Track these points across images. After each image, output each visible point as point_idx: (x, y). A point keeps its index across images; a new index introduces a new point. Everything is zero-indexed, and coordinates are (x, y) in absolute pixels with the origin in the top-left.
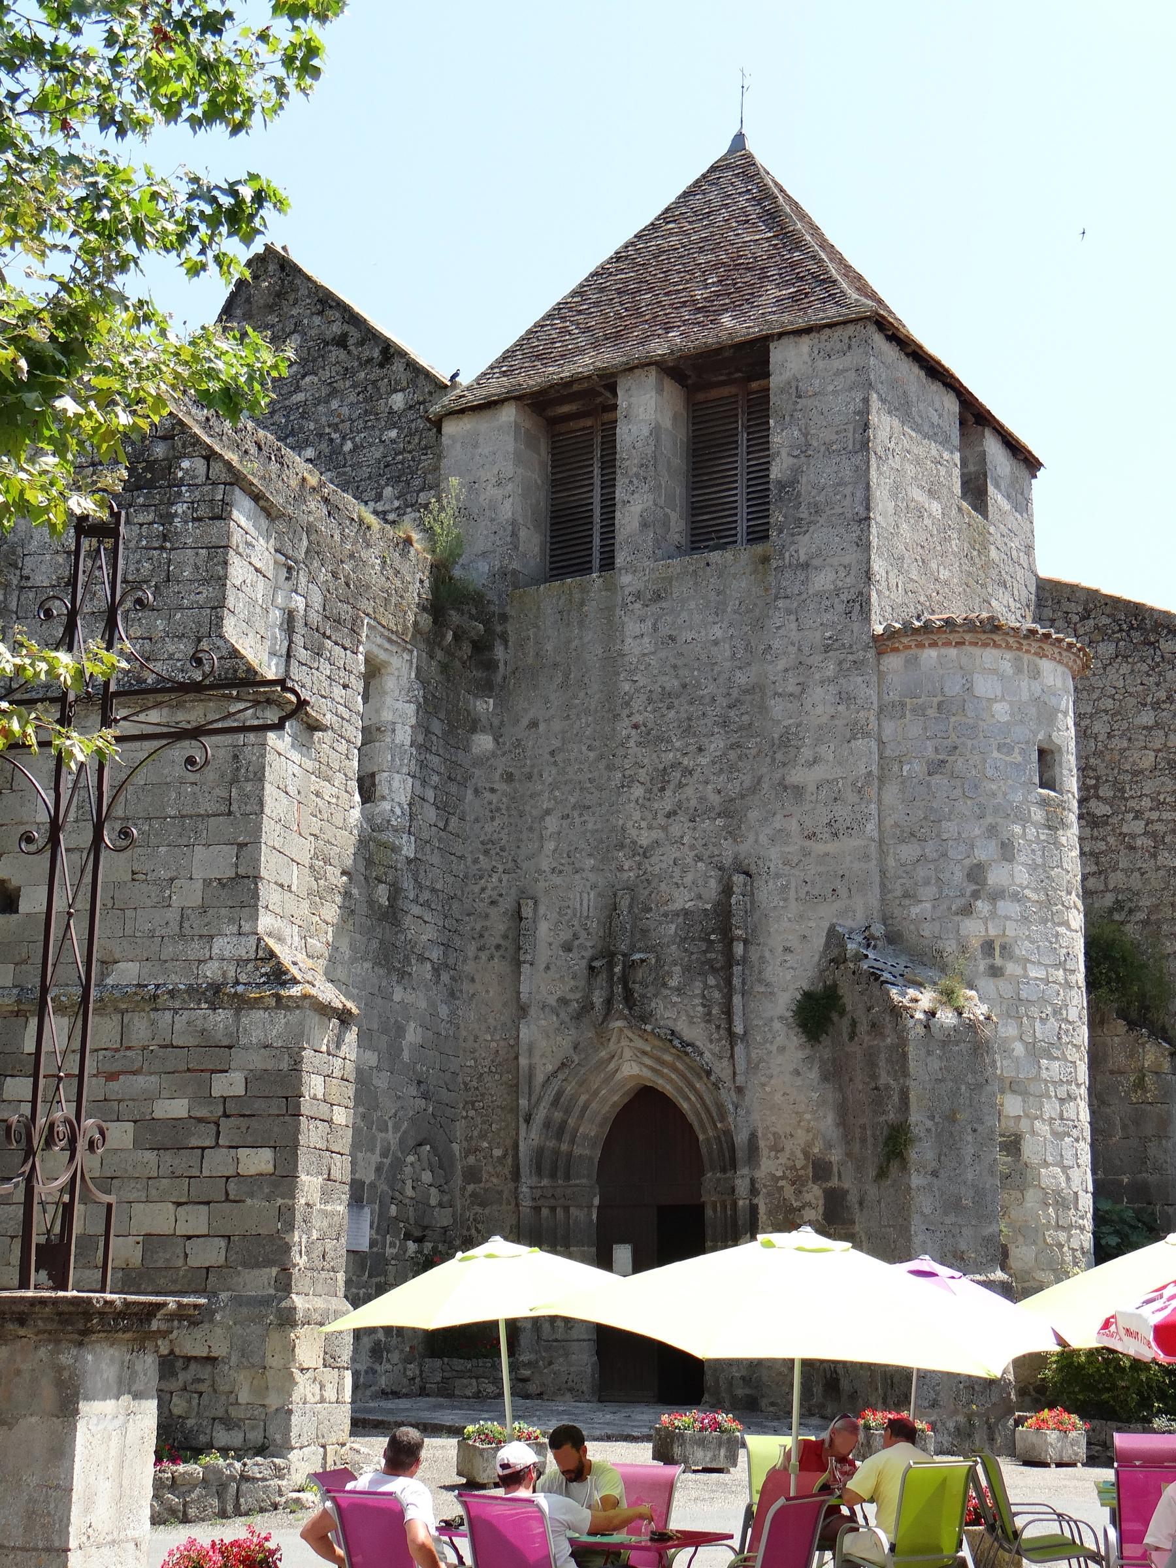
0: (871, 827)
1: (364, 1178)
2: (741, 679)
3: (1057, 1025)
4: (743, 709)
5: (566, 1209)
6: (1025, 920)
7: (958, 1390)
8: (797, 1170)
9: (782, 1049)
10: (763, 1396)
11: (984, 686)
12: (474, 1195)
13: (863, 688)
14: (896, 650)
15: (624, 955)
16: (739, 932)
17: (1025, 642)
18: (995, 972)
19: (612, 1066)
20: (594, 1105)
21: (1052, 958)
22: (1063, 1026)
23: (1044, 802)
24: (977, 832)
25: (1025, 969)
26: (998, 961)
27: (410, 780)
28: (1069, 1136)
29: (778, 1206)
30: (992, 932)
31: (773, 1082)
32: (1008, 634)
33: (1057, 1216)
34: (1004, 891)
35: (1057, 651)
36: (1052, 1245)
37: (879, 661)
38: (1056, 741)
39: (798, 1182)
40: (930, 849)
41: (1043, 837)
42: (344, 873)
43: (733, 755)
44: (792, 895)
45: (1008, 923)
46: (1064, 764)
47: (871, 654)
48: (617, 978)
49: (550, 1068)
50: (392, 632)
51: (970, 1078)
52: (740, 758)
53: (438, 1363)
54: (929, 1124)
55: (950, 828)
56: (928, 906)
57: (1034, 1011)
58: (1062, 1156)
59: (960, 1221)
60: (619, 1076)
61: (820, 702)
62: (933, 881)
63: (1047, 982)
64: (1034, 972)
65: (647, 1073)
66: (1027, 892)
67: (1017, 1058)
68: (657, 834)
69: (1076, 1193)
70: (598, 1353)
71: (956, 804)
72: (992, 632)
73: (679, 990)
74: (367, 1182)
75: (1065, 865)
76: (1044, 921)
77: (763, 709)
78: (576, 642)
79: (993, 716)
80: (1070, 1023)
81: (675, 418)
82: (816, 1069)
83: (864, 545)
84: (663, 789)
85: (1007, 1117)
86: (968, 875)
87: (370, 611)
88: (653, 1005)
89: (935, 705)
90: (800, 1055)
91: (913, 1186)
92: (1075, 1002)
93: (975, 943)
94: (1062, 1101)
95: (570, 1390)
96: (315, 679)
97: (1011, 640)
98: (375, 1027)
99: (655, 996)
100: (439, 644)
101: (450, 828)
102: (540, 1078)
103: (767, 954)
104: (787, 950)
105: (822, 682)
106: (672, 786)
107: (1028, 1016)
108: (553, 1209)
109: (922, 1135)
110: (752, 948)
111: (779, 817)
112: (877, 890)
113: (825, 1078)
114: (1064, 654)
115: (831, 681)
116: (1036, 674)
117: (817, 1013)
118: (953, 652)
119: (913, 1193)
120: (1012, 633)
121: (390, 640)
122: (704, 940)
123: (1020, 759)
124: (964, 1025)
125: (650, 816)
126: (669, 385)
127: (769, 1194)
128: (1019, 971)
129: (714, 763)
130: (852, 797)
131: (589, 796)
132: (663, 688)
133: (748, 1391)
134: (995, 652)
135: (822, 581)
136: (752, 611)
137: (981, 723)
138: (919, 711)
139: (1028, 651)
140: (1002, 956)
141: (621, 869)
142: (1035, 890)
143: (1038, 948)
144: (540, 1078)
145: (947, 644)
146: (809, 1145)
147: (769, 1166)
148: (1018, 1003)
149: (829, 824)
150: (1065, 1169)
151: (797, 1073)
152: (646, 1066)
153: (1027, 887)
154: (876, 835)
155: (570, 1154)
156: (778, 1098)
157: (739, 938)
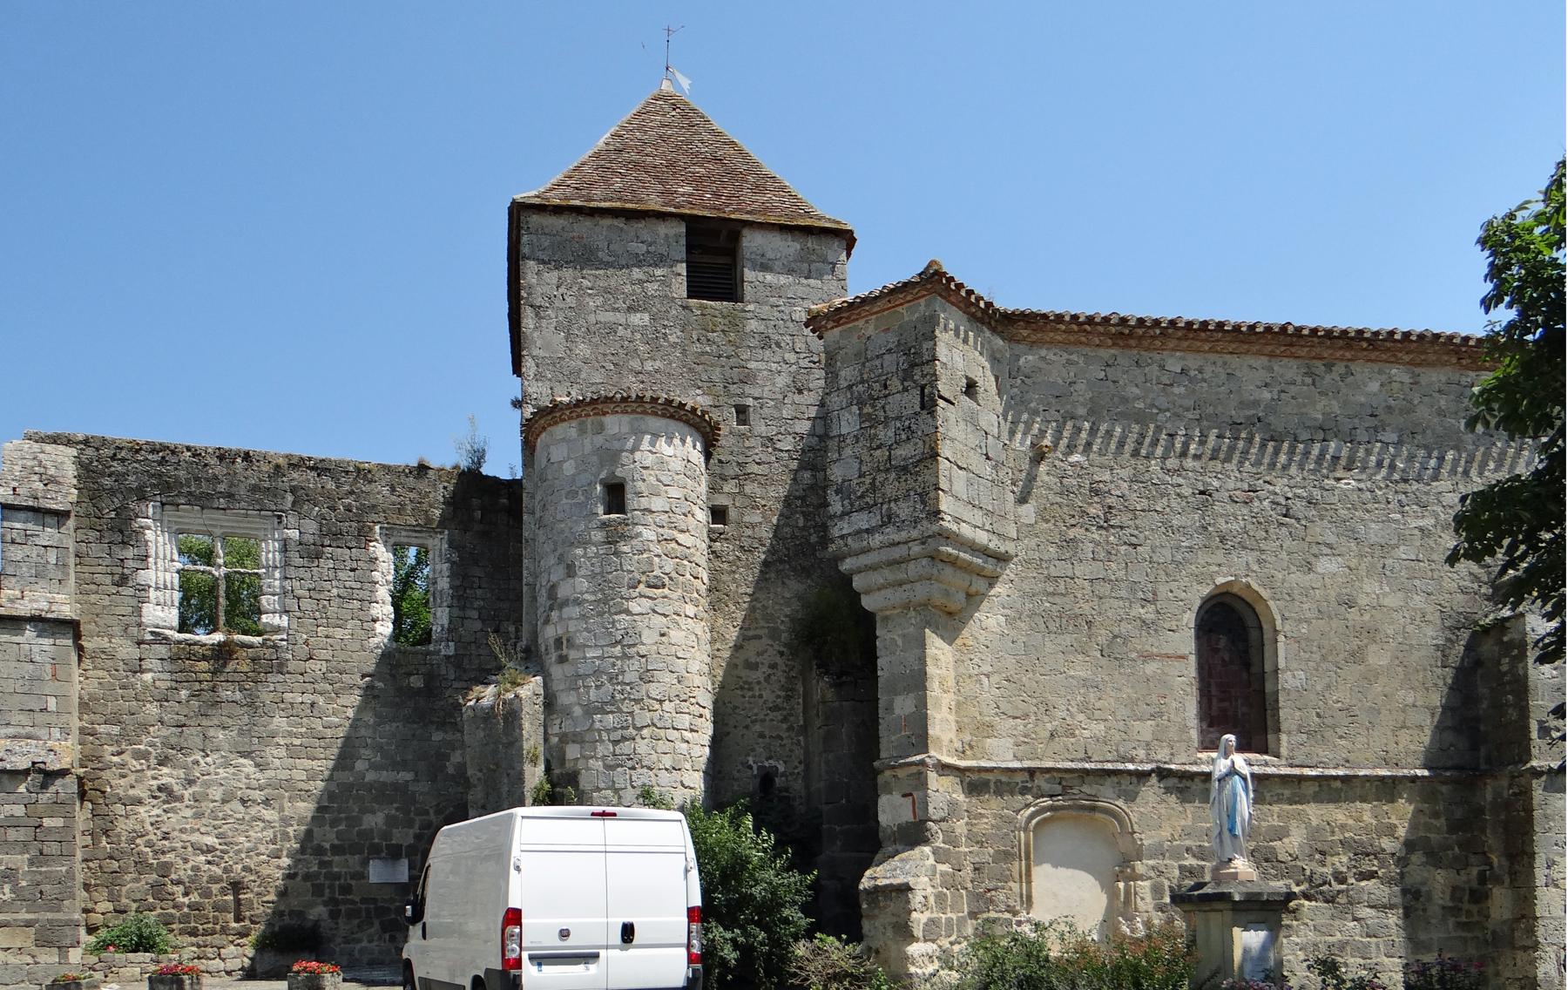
6: (584, 617)
26: (565, 652)
63: (601, 658)
66: (587, 596)
76: (601, 614)
134: (564, 424)
142: (594, 593)
150: (616, 791)
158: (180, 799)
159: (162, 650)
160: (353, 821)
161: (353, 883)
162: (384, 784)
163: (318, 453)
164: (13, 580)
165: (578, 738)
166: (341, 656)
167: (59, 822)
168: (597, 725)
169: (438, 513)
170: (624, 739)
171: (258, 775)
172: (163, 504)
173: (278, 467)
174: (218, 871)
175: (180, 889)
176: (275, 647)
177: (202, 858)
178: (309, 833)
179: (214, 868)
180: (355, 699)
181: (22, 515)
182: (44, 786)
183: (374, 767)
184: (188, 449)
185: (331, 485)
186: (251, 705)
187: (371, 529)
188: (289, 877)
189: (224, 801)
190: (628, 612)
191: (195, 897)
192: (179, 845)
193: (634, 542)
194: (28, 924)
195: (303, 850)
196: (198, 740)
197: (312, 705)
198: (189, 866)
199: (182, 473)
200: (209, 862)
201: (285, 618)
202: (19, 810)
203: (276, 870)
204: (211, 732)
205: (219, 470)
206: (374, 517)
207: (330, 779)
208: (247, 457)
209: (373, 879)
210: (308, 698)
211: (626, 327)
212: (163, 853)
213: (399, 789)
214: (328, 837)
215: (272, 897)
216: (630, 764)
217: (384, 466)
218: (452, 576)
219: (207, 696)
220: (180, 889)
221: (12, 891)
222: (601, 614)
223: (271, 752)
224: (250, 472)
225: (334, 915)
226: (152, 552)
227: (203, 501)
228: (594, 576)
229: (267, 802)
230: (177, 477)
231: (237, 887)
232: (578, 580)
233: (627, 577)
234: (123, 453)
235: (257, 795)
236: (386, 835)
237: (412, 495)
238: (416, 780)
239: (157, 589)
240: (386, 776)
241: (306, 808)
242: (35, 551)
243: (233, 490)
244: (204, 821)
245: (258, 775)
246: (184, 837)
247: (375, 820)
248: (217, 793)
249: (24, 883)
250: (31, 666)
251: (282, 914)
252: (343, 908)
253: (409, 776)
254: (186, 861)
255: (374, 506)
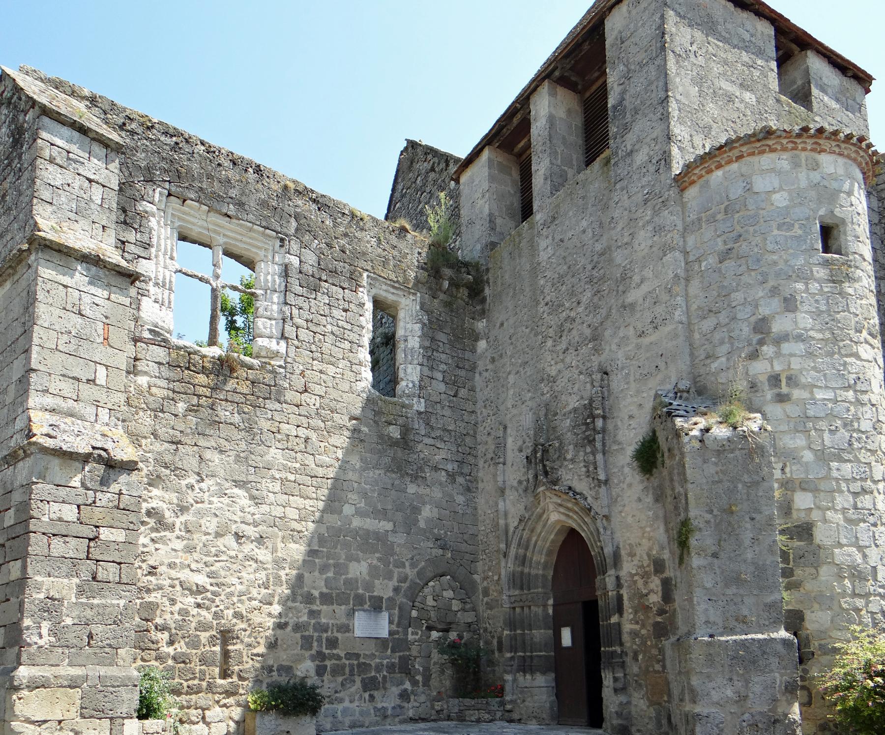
0: (678, 314)
1: (382, 595)
2: (598, 247)
3: (847, 435)
4: (600, 266)
5: (530, 607)
6: (810, 355)
7: (742, 728)
8: (644, 568)
9: (630, 485)
10: (632, 725)
11: (761, 184)
12: (487, 603)
13: (670, 217)
14: (693, 182)
15: (543, 445)
16: (598, 412)
17: (798, 141)
18: (782, 398)
19: (545, 516)
20: (539, 543)
21: (840, 382)
22: (855, 435)
23: (826, 263)
24: (761, 294)
25: (812, 393)
26: (785, 389)
27: (419, 367)
28: (865, 521)
29: (634, 594)
30: (778, 368)
31: (626, 509)
32: (780, 137)
33: (854, 586)
34: (787, 335)
35: (834, 143)
36: (847, 610)
37: (681, 196)
38: (838, 215)
39: (645, 576)
40: (723, 318)
41: (826, 290)
42: (352, 418)
43: (596, 299)
44: (632, 378)
45: (792, 359)
46: (849, 233)
47: (673, 193)
48: (543, 462)
49: (516, 524)
50: (394, 282)
51: (746, 478)
52: (600, 300)
53: (456, 701)
54: (708, 517)
55: (738, 297)
56: (724, 359)
57: (823, 425)
58: (857, 538)
59: (741, 592)
60: (549, 522)
61: (644, 239)
62: (727, 340)
63: (835, 401)
64: (820, 395)
65: (563, 518)
66: (811, 333)
67: (807, 463)
68: (560, 366)
69: (874, 568)
70: (557, 695)
71: (742, 277)
72: (765, 138)
73: (573, 461)
74: (385, 597)
75: (852, 310)
76: (831, 354)
77: (611, 260)
78: (518, 267)
79: (772, 204)
80: (863, 432)
81: (569, 112)
82: (651, 496)
83: (665, 118)
84: (561, 336)
85: (799, 510)
86: (754, 328)
87: (369, 268)
88: (560, 473)
89: (723, 210)
90: (641, 487)
91: (694, 566)
92: (867, 416)
93: (763, 378)
94: (856, 494)
95: (535, 717)
96: (312, 304)
97: (785, 141)
98: (390, 507)
99: (560, 467)
100: (440, 290)
101: (460, 395)
102: (512, 529)
103: (619, 423)
104: (631, 417)
105: (644, 226)
106: (565, 333)
107: (816, 429)
108: (522, 608)
109: (701, 526)
110: (609, 421)
111: (622, 329)
112: (687, 359)
113: (657, 500)
114: (843, 145)
115: (648, 222)
116: (816, 166)
117: (649, 456)
118: (735, 166)
119: (695, 572)
120: (784, 134)
121: (394, 287)
122: (583, 424)
123: (800, 232)
124: (738, 436)
125: (555, 356)
126: (561, 91)
127: (629, 587)
128: (805, 395)
129: (586, 308)
130: (664, 297)
131: (527, 356)
132: (559, 274)
133: (620, 722)
134: (773, 155)
135: (640, 158)
136: (602, 200)
137: (761, 212)
138: (712, 220)
139: (804, 149)
140: (788, 385)
141: (543, 394)
142: (820, 331)
143: (825, 375)
144: (512, 529)
145: (730, 162)
146: (651, 549)
147: (628, 567)
148: (805, 420)
149: (652, 322)
150: (860, 548)
151: (640, 500)
152: (563, 514)
153: (812, 329)
154: (684, 319)
155: (529, 574)
156: (630, 520)
157: (598, 416)
158: (171, 528)
159: (160, 353)
160: (340, 569)
161: (339, 635)
162: (368, 531)
163: (320, 188)
164: (49, 208)
165: (805, 486)
166: (334, 394)
167: (120, 536)
168: (835, 474)
169: (413, 275)
170: (864, 491)
171: (252, 509)
172: (170, 195)
173: (286, 187)
174: (207, 616)
175: (166, 636)
176: (273, 372)
177: (190, 600)
178: (300, 578)
179: (204, 612)
180: (342, 440)
181: (66, 131)
182: (104, 482)
183: (359, 513)
184: (203, 143)
185: (328, 222)
186: (249, 430)
187: (361, 275)
188: (280, 626)
189: (218, 535)
190: (857, 356)
191: (181, 647)
192: (167, 582)
193: (857, 285)
194: (73, 684)
195: (293, 597)
196: (194, 462)
197: (307, 440)
198: (176, 608)
199: (195, 166)
200: (199, 606)
201: (283, 344)
202: (70, 513)
203: (266, 619)
204: (208, 455)
205: (232, 174)
206: (362, 263)
207: (319, 522)
208: (258, 170)
209: (358, 633)
210: (302, 432)
211: (742, 101)
212: (149, 591)
213: (381, 537)
214: (317, 584)
215: (261, 649)
216: (872, 519)
217: (372, 218)
218: (423, 336)
219: (205, 412)
220: (166, 636)
221: (52, 632)
222: (831, 354)
223: (266, 484)
224: (260, 186)
225: (320, 671)
226: (154, 241)
227: (212, 201)
228: (819, 313)
229: (260, 540)
230: (189, 171)
231: (226, 636)
232: (800, 316)
233: (854, 320)
234: (134, 126)
235: (250, 531)
236: (369, 587)
237: (395, 253)
238: (394, 531)
239: (157, 284)
240: (370, 524)
241: (297, 550)
242: (78, 182)
243: (244, 199)
244: (196, 556)
245: (252, 509)
246: (173, 573)
247: (359, 569)
248: (211, 524)
249: (69, 621)
250: (79, 320)
251: (270, 669)
252: (328, 663)
253: (389, 526)
254: (173, 602)
255: (364, 254)
